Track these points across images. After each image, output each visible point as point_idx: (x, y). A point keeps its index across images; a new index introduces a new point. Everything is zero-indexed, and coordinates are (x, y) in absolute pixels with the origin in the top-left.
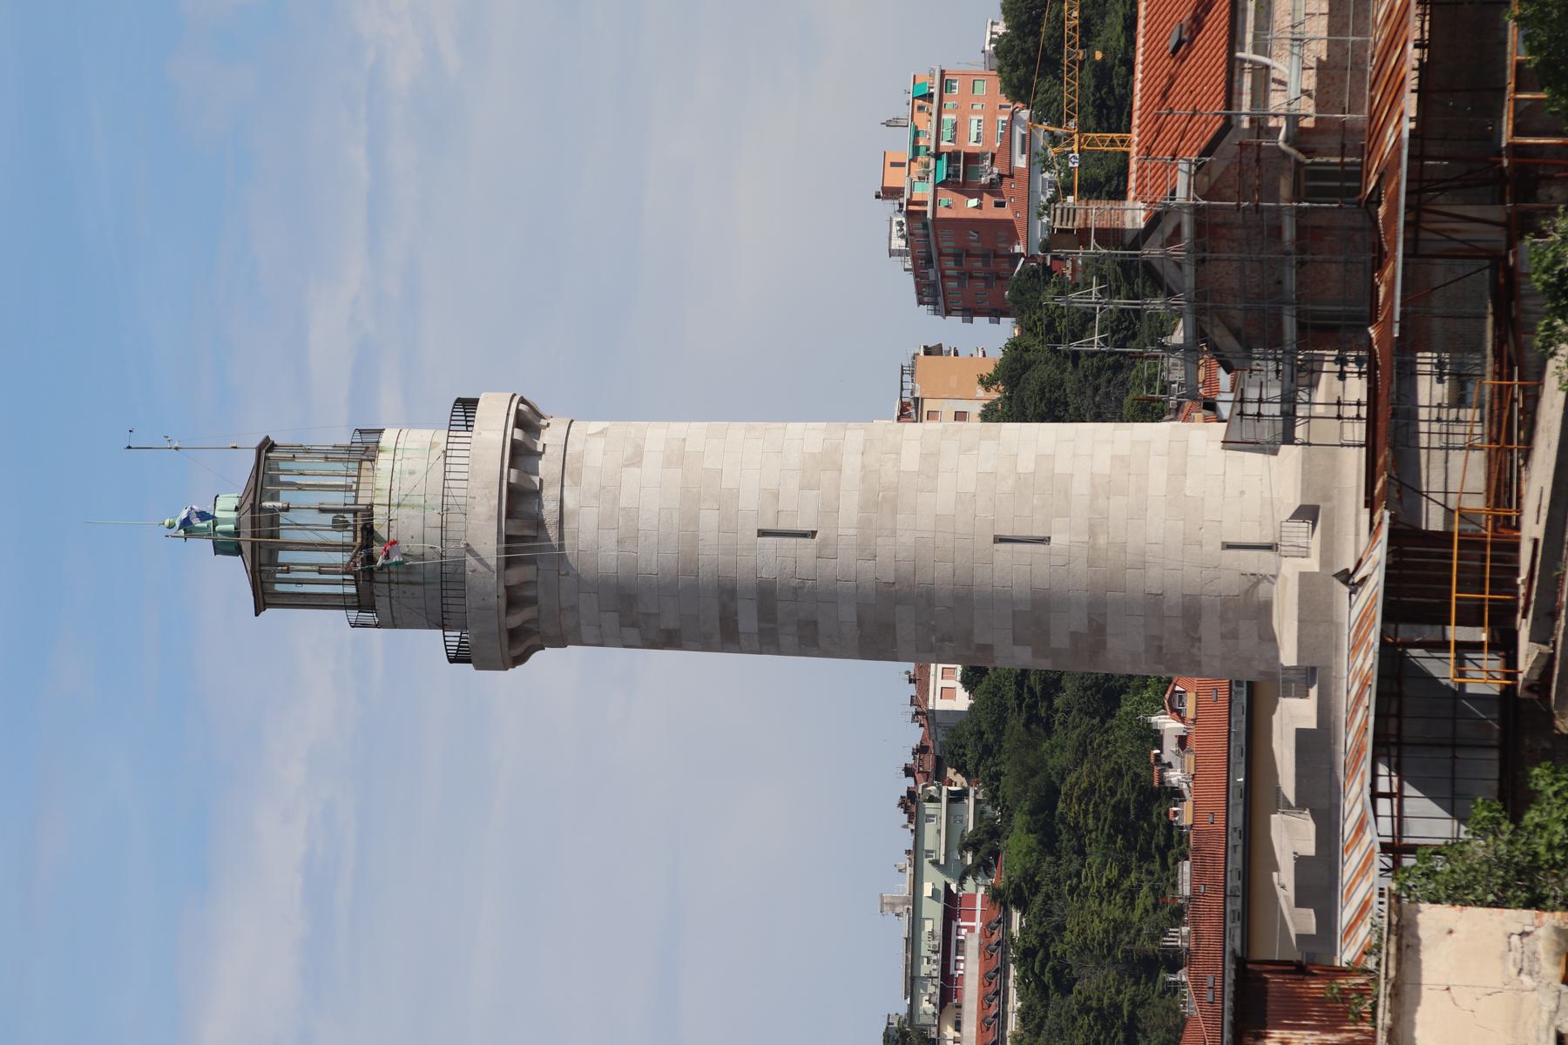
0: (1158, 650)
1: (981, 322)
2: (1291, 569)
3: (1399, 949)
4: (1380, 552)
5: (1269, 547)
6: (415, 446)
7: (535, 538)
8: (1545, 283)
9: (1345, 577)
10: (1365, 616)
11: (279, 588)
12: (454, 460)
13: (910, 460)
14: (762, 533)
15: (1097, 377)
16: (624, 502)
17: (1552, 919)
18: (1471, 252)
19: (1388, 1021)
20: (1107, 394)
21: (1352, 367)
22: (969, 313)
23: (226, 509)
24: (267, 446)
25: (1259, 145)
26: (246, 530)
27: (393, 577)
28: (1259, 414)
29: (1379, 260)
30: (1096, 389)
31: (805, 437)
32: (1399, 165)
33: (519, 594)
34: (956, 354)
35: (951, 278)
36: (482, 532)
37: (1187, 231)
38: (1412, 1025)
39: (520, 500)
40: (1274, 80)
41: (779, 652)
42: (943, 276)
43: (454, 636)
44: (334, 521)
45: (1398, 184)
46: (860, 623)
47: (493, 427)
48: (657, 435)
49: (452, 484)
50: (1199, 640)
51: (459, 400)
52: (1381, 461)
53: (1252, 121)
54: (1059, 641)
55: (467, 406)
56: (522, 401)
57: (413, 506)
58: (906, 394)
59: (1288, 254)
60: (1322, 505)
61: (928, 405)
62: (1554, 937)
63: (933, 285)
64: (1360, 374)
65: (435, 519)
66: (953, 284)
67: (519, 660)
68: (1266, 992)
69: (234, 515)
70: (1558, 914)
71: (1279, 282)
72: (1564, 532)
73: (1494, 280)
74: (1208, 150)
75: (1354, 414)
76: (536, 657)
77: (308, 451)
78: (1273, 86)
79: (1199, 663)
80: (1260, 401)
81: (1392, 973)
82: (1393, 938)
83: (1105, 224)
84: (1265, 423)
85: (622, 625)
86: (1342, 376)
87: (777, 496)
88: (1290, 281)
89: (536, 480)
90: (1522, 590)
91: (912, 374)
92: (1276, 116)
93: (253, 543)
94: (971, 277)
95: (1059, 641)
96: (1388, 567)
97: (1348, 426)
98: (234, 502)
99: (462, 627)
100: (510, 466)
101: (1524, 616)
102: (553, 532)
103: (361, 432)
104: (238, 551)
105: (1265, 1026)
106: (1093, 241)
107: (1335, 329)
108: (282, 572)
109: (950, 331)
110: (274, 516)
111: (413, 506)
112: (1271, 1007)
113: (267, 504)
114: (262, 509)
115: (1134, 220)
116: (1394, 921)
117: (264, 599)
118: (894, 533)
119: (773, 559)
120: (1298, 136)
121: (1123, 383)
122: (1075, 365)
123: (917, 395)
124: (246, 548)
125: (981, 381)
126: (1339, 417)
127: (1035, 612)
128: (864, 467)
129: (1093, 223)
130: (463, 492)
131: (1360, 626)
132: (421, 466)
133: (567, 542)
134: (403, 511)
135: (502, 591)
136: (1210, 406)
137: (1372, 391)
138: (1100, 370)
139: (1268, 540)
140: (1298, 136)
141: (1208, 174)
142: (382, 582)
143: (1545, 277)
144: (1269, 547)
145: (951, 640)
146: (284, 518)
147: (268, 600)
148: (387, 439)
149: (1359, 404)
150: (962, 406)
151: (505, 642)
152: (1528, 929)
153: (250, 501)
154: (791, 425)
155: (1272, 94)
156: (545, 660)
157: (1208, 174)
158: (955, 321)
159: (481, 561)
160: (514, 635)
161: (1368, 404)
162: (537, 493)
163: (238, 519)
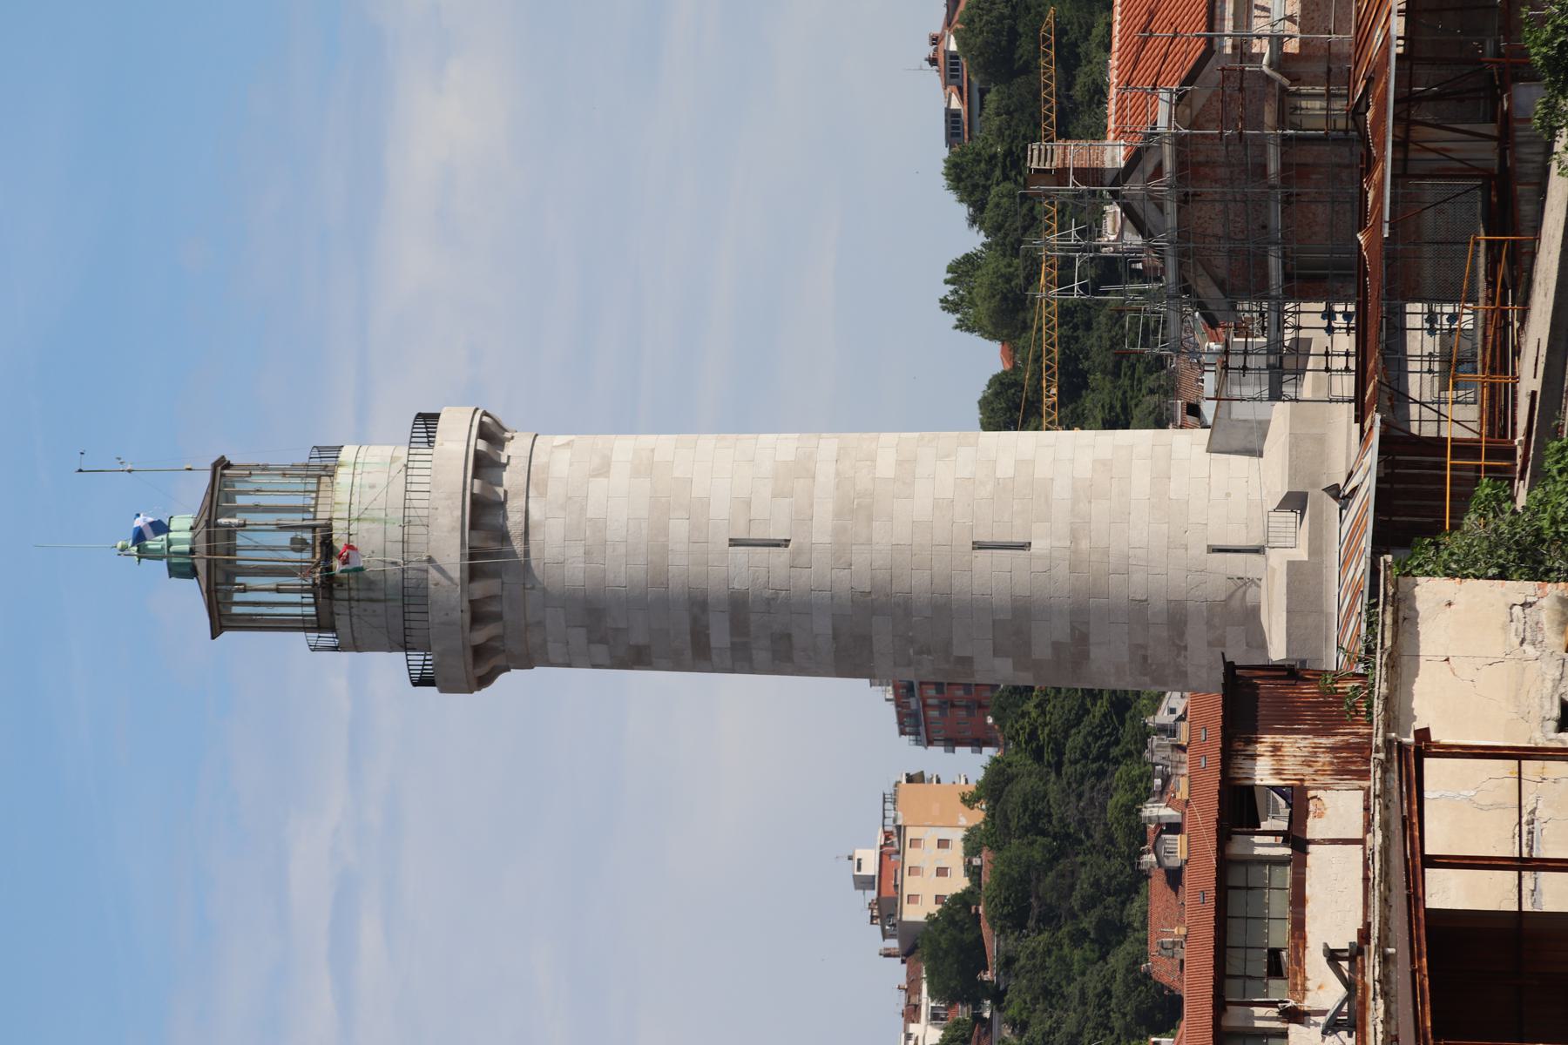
0: (1143, 661)
1: (963, 752)
2: (1277, 561)
3: (1395, 622)
4: (1372, 458)
5: (1258, 550)
6: (375, 460)
7: (498, 554)
8: (1545, 57)
9: (1334, 491)
10: (1358, 524)
11: (236, 610)
12: (415, 472)
13: (886, 466)
14: (734, 543)
15: (1081, 783)
16: (591, 513)
17: (1554, 590)
18: (1468, 171)
19: (1384, 690)
20: (1092, 800)
21: (1340, 321)
22: (951, 743)
23: (182, 528)
24: (222, 465)
25: (1242, 70)
26: (202, 546)
27: (354, 594)
28: (1245, 368)
29: (1368, 164)
30: (1080, 797)
31: (777, 447)
32: (1388, 63)
33: (481, 613)
34: (938, 781)
35: (933, 707)
36: (446, 543)
37: (1168, 165)
38: (1411, 696)
39: (484, 511)
40: (1257, 7)
41: (752, 671)
42: (925, 705)
43: (417, 658)
44: (293, 540)
45: (1387, 83)
46: (835, 637)
47: (456, 438)
48: (624, 447)
49: (413, 495)
50: (1185, 648)
51: (419, 415)
52: (1371, 366)
53: (1234, 47)
54: (1042, 651)
55: (428, 420)
56: (485, 414)
57: (373, 520)
58: (889, 822)
59: (1273, 187)
60: (1310, 491)
61: (911, 833)
62: (1558, 607)
63: (914, 715)
64: (1348, 330)
65: (395, 533)
66: (934, 713)
67: (484, 681)
68: (1256, 697)
69: (188, 535)
70: (1562, 585)
71: (1264, 227)
72: (1563, 378)
73: (1487, 203)
74: (1190, 79)
75: (1343, 366)
76: (503, 678)
77: (265, 468)
78: (1256, 12)
79: (1185, 674)
80: (1246, 353)
81: (1388, 643)
82: (1389, 609)
83: (1084, 164)
84: (1251, 377)
85: (590, 641)
86: (1330, 330)
87: (748, 504)
88: (1275, 218)
89: (500, 491)
90: (1520, 451)
91: (895, 802)
92: (1259, 37)
93: (209, 561)
94: (953, 706)
95: (1042, 651)
96: (1379, 480)
97: (1336, 379)
98: (189, 522)
99: (427, 648)
100: (475, 476)
101: (1522, 478)
102: (518, 546)
103: (318, 448)
104: (192, 573)
105: (1255, 731)
106: (1072, 178)
107: (1324, 278)
108: (239, 591)
109: (934, 759)
110: (230, 532)
111: (373, 520)
112: (1262, 712)
113: (222, 521)
114: (217, 526)
115: (1113, 159)
116: (1391, 591)
117: (221, 621)
118: (869, 542)
119: (744, 570)
120: (1282, 61)
121: (1107, 789)
122: (1059, 774)
123: (899, 822)
124: (201, 567)
125: (964, 800)
126: (1327, 370)
127: (1015, 622)
128: (838, 474)
129: (1071, 163)
130: (425, 504)
131: (1350, 543)
132: (381, 480)
133: (532, 555)
134: (365, 526)
135: (466, 605)
136: (1194, 410)
137: (1361, 342)
138: (1083, 776)
139: (1255, 542)
140: (1282, 61)
141: (1190, 106)
142: (345, 600)
143: (1544, 50)
144: (1258, 550)
145: (929, 652)
146: (240, 540)
147: (225, 623)
148: (347, 454)
149: (1347, 354)
150: (944, 834)
151: (470, 660)
152: (1530, 599)
153: (206, 517)
154: (762, 436)
155: (1255, 21)
156: (511, 681)
157: (1190, 106)
158: (937, 751)
159: (441, 570)
160: (479, 653)
161: (1357, 355)
162: (502, 505)
163: (193, 540)
